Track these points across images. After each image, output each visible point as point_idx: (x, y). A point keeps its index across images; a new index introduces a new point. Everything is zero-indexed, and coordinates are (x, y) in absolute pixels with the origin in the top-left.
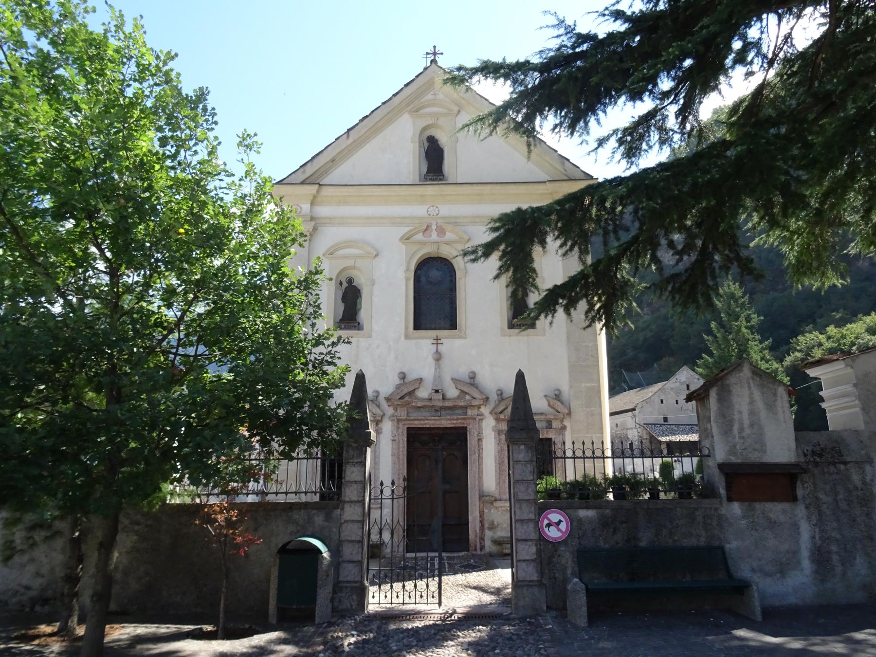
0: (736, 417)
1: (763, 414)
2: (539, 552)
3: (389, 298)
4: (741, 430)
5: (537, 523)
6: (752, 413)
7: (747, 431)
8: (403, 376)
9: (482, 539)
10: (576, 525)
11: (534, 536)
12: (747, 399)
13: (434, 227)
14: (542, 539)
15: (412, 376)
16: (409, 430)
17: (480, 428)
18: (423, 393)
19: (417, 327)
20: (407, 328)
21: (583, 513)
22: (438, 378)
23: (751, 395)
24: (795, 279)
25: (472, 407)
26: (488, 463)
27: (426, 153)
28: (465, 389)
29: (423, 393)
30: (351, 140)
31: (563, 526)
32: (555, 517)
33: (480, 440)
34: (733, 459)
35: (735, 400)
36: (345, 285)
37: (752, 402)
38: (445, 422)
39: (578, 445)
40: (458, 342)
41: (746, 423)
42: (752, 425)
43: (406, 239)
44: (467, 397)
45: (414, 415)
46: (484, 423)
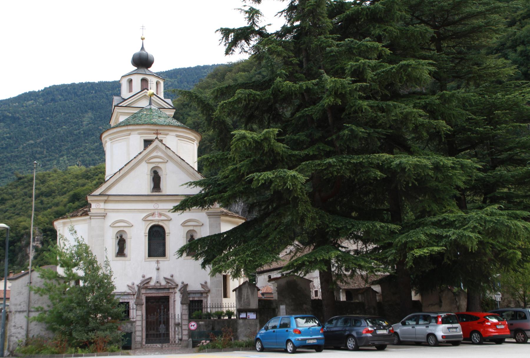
0: (243, 296)
1: (250, 296)
2: (189, 333)
3: (138, 243)
4: (244, 300)
5: (188, 325)
6: (247, 295)
7: (245, 300)
8: (144, 277)
9: (175, 338)
10: (199, 326)
11: (187, 328)
12: (246, 292)
13: (157, 213)
14: (189, 330)
15: (147, 277)
16: (146, 297)
17: (174, 297)
18: (152, 283)
19: (150, 255)
20: (145, 257)
21: (201, 323)
22: (158, 277)
23: (248, 291)
24: (423, 179)
25: (171, 288)
26: (177, 309)
27: (153, 179)
28: (169, 281)
29: (152, 283)
30: (121, 175)
31: (195, 326)
32: (193, 323)
33: (174, 301)
34: (241, 308)
35: (243, 292)
36: (119, 238)
37: (248, 293)
38: (161, 294)
39: (227, 304)
40: (166, 263)
41: (245, 297)
42: (247, 299)
43: (145, 220)
44: (170, 285)
45: (148, 292)
46: (176, 295)
